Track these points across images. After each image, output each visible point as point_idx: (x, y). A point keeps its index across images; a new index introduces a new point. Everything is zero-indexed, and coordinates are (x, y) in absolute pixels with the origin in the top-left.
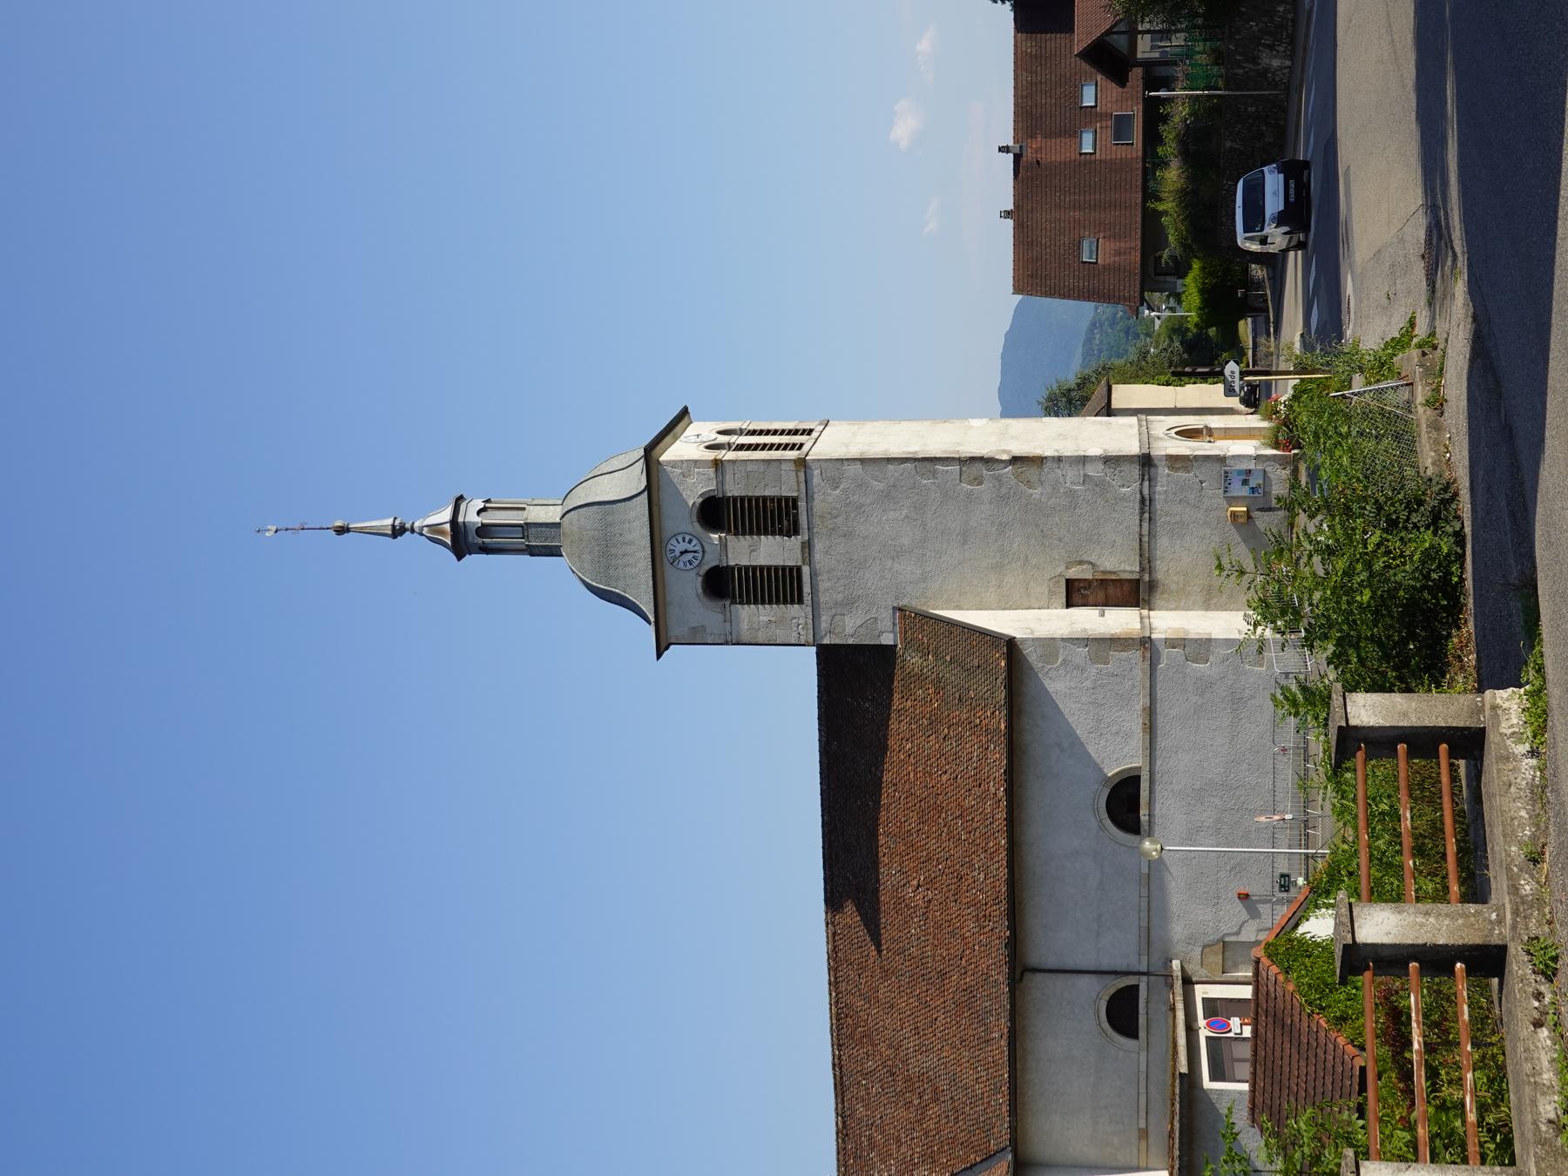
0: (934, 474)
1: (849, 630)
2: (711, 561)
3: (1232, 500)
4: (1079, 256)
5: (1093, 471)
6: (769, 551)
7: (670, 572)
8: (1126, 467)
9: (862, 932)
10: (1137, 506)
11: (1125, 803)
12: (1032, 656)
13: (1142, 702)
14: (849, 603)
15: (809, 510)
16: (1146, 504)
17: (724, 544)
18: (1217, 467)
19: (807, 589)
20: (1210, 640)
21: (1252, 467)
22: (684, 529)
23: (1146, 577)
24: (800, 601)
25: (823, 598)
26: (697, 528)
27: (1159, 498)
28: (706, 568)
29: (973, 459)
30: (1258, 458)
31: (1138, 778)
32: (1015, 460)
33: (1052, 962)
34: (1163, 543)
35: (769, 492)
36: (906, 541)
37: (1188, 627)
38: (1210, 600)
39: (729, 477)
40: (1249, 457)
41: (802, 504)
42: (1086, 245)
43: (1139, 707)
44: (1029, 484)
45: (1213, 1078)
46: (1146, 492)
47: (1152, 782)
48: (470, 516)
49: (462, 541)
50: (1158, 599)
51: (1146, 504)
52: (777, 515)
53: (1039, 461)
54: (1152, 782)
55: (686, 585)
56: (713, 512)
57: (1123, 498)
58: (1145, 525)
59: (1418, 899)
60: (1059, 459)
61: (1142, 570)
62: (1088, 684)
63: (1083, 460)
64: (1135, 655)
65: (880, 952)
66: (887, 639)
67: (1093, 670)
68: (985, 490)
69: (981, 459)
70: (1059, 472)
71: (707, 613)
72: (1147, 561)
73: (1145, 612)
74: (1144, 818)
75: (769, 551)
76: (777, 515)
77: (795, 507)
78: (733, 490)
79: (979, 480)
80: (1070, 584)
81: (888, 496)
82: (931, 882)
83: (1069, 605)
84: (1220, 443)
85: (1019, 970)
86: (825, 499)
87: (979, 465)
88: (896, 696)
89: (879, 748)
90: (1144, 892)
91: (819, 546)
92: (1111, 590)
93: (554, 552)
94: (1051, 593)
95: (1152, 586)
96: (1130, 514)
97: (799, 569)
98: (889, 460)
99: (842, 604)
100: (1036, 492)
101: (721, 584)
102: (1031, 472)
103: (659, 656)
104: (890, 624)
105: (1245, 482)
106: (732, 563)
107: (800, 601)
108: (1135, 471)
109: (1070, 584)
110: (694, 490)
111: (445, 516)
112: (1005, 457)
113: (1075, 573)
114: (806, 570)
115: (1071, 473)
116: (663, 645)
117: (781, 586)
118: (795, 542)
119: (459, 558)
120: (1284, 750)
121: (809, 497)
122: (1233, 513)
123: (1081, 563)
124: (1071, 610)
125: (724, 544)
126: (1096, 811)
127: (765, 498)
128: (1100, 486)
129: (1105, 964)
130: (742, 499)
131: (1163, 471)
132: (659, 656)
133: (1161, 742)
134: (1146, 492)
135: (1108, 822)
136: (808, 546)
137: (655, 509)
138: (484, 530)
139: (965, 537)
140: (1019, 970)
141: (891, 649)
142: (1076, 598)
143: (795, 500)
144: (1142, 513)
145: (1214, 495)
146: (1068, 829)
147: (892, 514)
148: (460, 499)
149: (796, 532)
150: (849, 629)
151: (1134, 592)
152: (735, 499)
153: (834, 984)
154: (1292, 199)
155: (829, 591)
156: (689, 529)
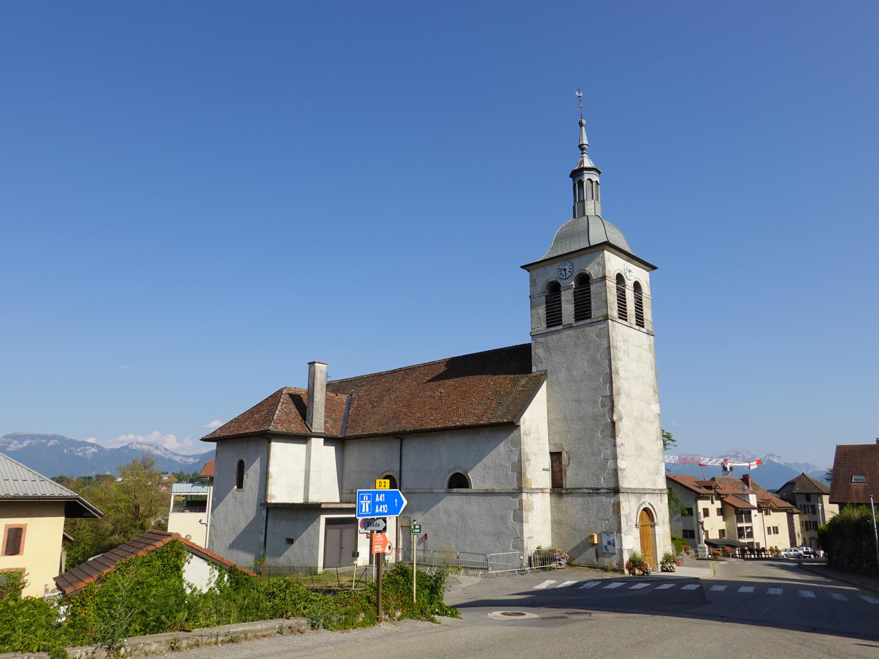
0: (605, 383)
1: (537, 351)
2: (563, 283)
3: (600, 535)
4: (855, 474)
5: (610, 462)
6: (568, 309)
7: (556, 266)
8: (613, 480)
9: (436, 374)
10: (595, 486)
11: (459, 481)
12: (514, 435)
13: (496, 488)
14: (548, 350)
15: (585, 325)
16: (596, 491)
17: (570, 287)
18: (616, 528)
19: (553, 329)
20: (522, 522)
21: (616, 547)
22: (575, 267)
23: (564, 492)
24: (548, 327)
25: (549, 338)
26: (576, 274)
27: (599, 498)
28: (559, 281)
29: (613, 402)
30: (621, 551)
31: (467, 487)
32: (613, 423)
33: (404, 451)
34: (580, 500)
35: (593, 305)
36: (575, 373)
37: (534, 512)
38: (557, 524)
39: (599, 285)
40: (621, 546)
41: (588, 321)
42: (862, 477)
43: (495, 487)
44: (603, 431)
45: (329, 522)
46: (602, 491)
47: (467, 494)
48: (587, 176)
49: (577, 174)
50: (555, 498)
51: (596, 491)
52: (583, 311)
53: (614, 435)
54: (467, 494)
55: (551, 274)
56: (584, 280)
57: (598, 479)
58: (586, 491)
59: (38, 651)
60: (615, 446)
61: (567, 489)
62: (503, 463)
63: (615, 458)
64: (515, 486)
65: (429, 381)
66: (534, 369)
67: (509, 464)
68: (599, 409)
69: (613, 406)
70: (609, 446)
71: (541, 286)
72: (571, 492)
73: (549, 491)
74: (455, 490)
75: (568, 309)
76: (583, 311)
77: (586, 318)
78: (593, 288)
79: (603, 406)
80: (560, 454)
81: (594, 362)
82: (440, 398)
83: (552, 454)
84: (636, 533)
85: (400, 436)
86: (591, 332)
87: (610, 405)
88: (512, 376)
89: (495, 372)
90: (427, 491)
91: (571, 332)
92: (559, 474)
93: (574, 217)
94: (555, 445)
95: (560, 495)
96: (591, 483)
97: (561, 324)
98: (610, 360)
99: (547, 346)
100: (599, 435)
101: (554, 289)
102: (608, 432)
103: (523, 267)
104: (540, 369)
105: (609, 543)
106: (562, 293)
107: (548, 327)
108: (612, 485)
109: (560, 454)
110: (592, 270)
111: (587, 163)
112: (615, 418)
113: (565, 456)
114: (561, 327)
115: (609, 452)
116: (529, 268)
117: (554, 318)
118: (571, 320)
119: (571, 176)
120: (458, 557)
121: (592, 324)
122: (592, 537)
123: (569, 459)
124: (548, 456)
125: (570, 287)
126: (455, 468)
127: (590, 303)
128: (603, 468)
129: (404, 474)
130: (589, 292)
131: (612, 500)
132: (523, 267)
133: (481, 498)
134: (602, 491)
135: (451, 474)
136: (570, 327)
137: (582, 252)
138: (581, 183)
139: (578, 401)
140: (400, 436)
141: (529, 371)
142: (555, 457)
143: (590, 317)
144: (592, 489)
145: (603, 526)
146: (446, 456)
147: (586, 364)
148: (599, 172)
149: (577, 320)
150: (538, 352)
151: (558, 487)
152: (589, 289)
153: (424, 365)
154: (586, 586)
155: (552, 339)
156: (575, 270)
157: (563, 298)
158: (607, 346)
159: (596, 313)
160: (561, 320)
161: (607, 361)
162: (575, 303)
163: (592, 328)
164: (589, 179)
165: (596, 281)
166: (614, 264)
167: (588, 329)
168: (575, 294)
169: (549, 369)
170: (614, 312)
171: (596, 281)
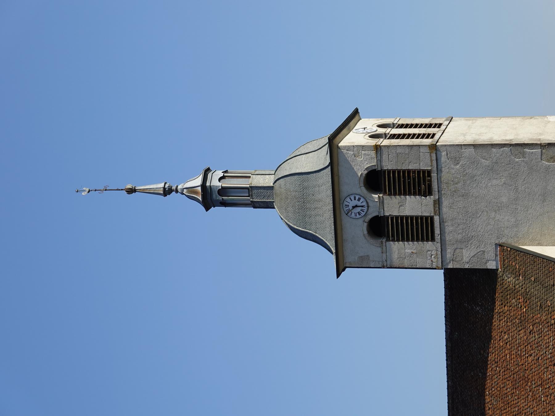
0: (523, 155)
1: (465, 259)
2: (373, 213)
6: (412, 206)
14: (466, 241)
17: (382, 202)
19: (437, 231)
24: (433, 240)
25: (448, 237)
26: (364, 191)
28: (370, 217)
36: (504, 199)
41: (434, 175)
48: (214, 182)
55: (356, 229)
56: (375, 180)
66: (492, 265)
75: (412, 206)
76: (417, 182)
78: (388, 165)
86: (449, 171)
88: (498, 303)
89: (486, 338)
91: (445, 203)
93: (269, 205)
97: (432, 218)
98: (493, 145)
99: (461, 242)
101: (379, 228)
103: (338, 275)
106: (387, 214)
107: (433, 240)
110: (362, 166)
111: (197, 182)
114: (436, 218)
116: (341, 268)
117: (420, 229)
118: (429, 200)
119: (207, 209)
127: (409, 171)
132: (338, 275)
136: (438, 203)
138: (223, 191)
141: (491, 274)
143: (429, 172)
147: (494, 182)
148: (208, 170)
150: (466, 259)
152: (389, 171)
155: (452, 233)
156: (358, 191)
157: (396, 213)
158: (472, 149)
159: (424, 163)
160: (427, 218)
161: (494, 150)
162: (405, 194)
163: (445, 170)
164: (220, 180)
165: (380, 161)
166: (355, 138)
167: (445, 175)
168: (393, 192)
169: (495, 240)
170: (427, 141)
171: (380, 161)
